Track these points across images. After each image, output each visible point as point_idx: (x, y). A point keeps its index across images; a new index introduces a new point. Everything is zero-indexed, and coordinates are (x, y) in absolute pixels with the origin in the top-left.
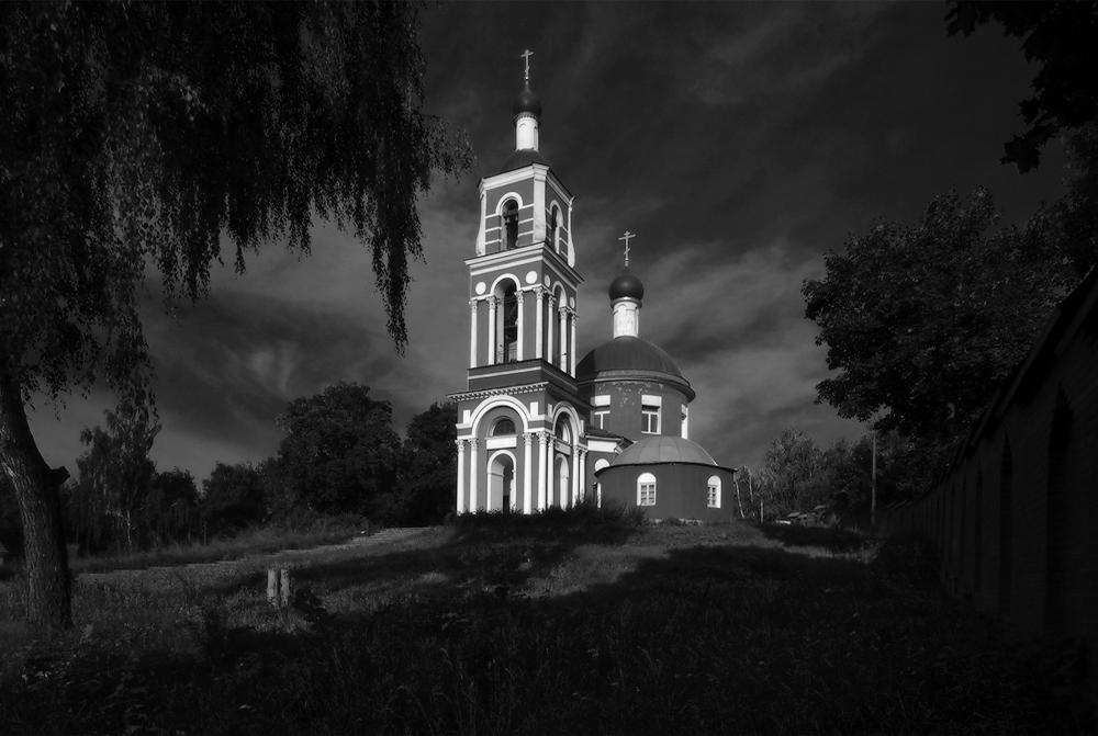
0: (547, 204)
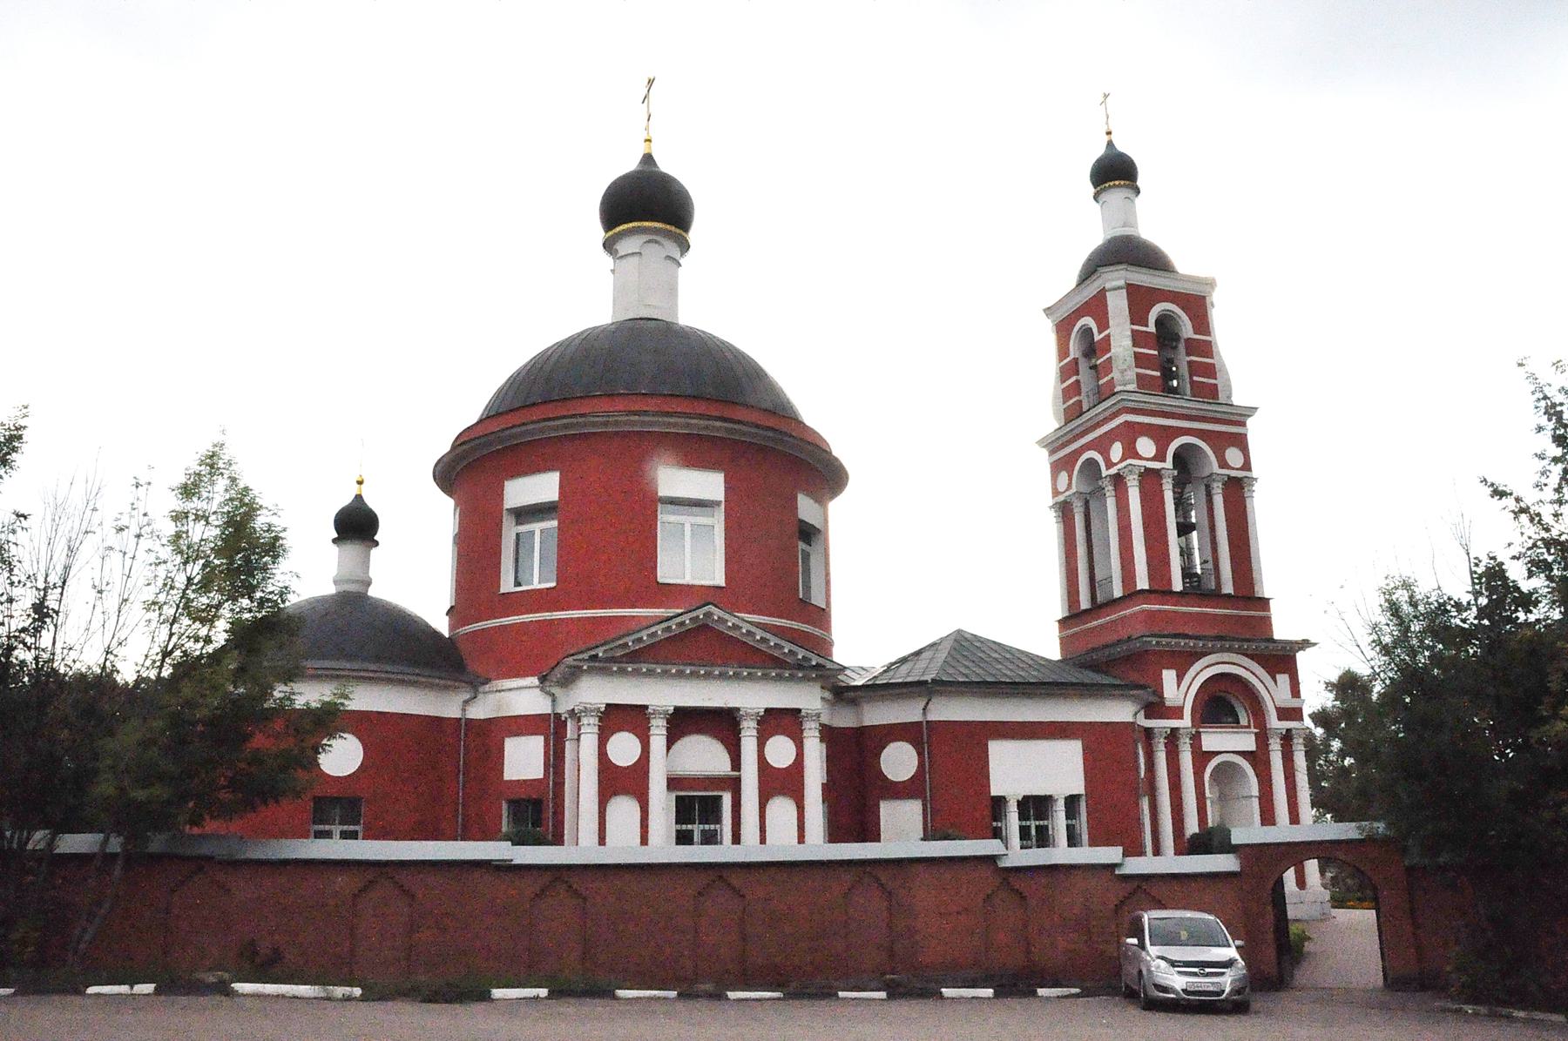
0: (1137, 316)
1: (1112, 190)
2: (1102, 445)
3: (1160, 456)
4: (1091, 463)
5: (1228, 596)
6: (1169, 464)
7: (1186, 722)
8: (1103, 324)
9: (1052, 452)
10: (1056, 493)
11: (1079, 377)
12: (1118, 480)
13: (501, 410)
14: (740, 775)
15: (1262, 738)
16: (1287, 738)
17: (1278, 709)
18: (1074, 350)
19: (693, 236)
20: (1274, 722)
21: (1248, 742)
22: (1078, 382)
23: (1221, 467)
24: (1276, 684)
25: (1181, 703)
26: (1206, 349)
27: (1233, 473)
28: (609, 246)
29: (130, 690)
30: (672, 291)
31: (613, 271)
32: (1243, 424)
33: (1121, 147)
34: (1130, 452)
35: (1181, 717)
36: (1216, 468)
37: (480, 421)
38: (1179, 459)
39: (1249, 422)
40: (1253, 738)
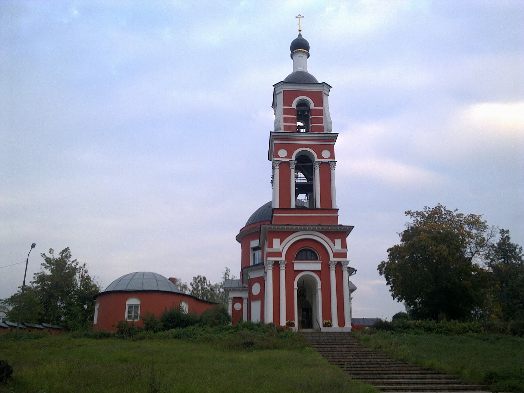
1: (295, 54)
3: (289, 156)
5: (318, 209)
7: (283, 258)
13: (254, 222)
15: (326, 266)
20: (332, 258)
21: (317, 266)
24: (280, 245)
26: (321, 112)
29: (247, 322)
33: (304, 37)
37: (245, 227)
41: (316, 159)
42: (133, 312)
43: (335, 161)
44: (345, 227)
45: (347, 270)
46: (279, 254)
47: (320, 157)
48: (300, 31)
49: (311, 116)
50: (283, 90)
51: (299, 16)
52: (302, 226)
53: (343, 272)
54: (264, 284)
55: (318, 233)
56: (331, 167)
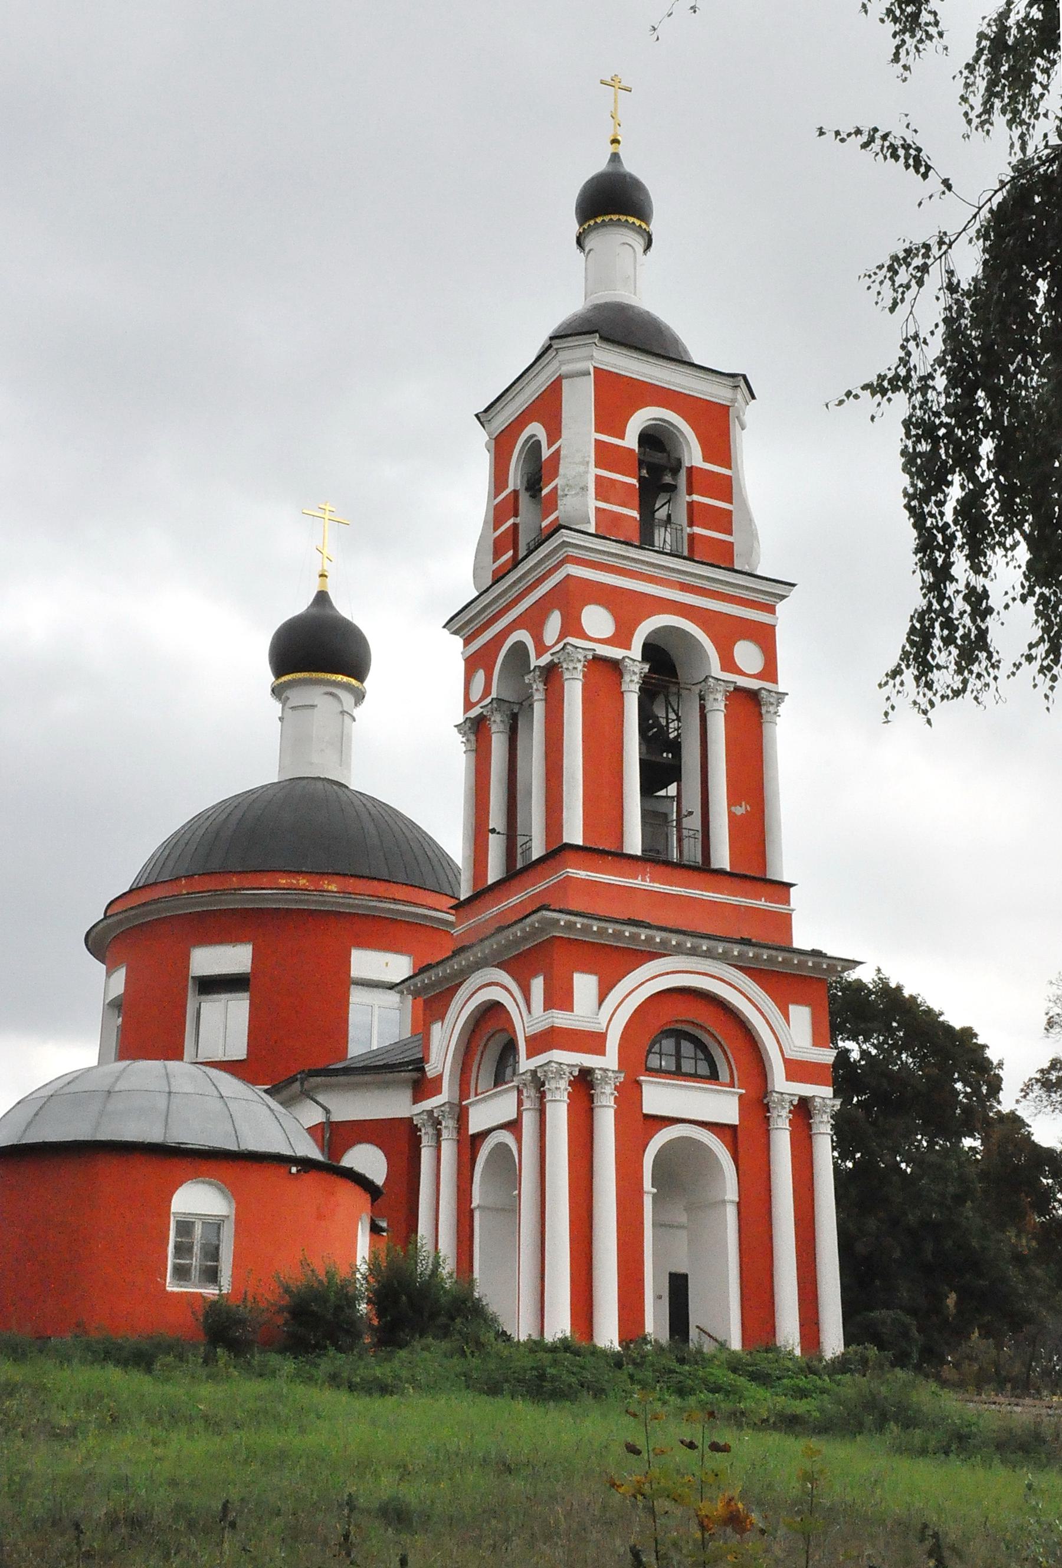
2: (534, 621)
3: (622, 638)
4: (519, 648)
5: (721, 872)
6: (636, 651)
7: (608, 1061)
8: (554, 432)
9: (467, 642)
10: (468, 705)
11: (518, 520)
12: (551, 674)
14: (217, 1267)
16: (803, 1109)
17: (787, 1062)
18: (515, 480)
19: (371, 683)
20: (780, 1082)
22: (515, 526)
23: (724, 668)
24: (789, 1025)
25: (604, 1031)
26: (725, 488)
27: (743, 682)
28: (277, 692)
30: (341, 744)
31: (281, 719)
32: (771, 609)
34: (572, 627)
35: (601, 1051)
36: (715, 667)
38: (652, 651)
39: (780, 607)
40: (736, 1099)
41: (715, 667)
42: (196, 1249)
43: (780, 690)
44: (834, 962)
45: (612, 1107)
46: (594, 1042)
47: (729, 664)
48: (615, 141)
49: (690, 493)
50: (595, 367)
51: (612, 83)
52: (671, 931)
53: (771, 1136)
54: (7, 1116)
55: (732, 970)
56: (763, 711)
